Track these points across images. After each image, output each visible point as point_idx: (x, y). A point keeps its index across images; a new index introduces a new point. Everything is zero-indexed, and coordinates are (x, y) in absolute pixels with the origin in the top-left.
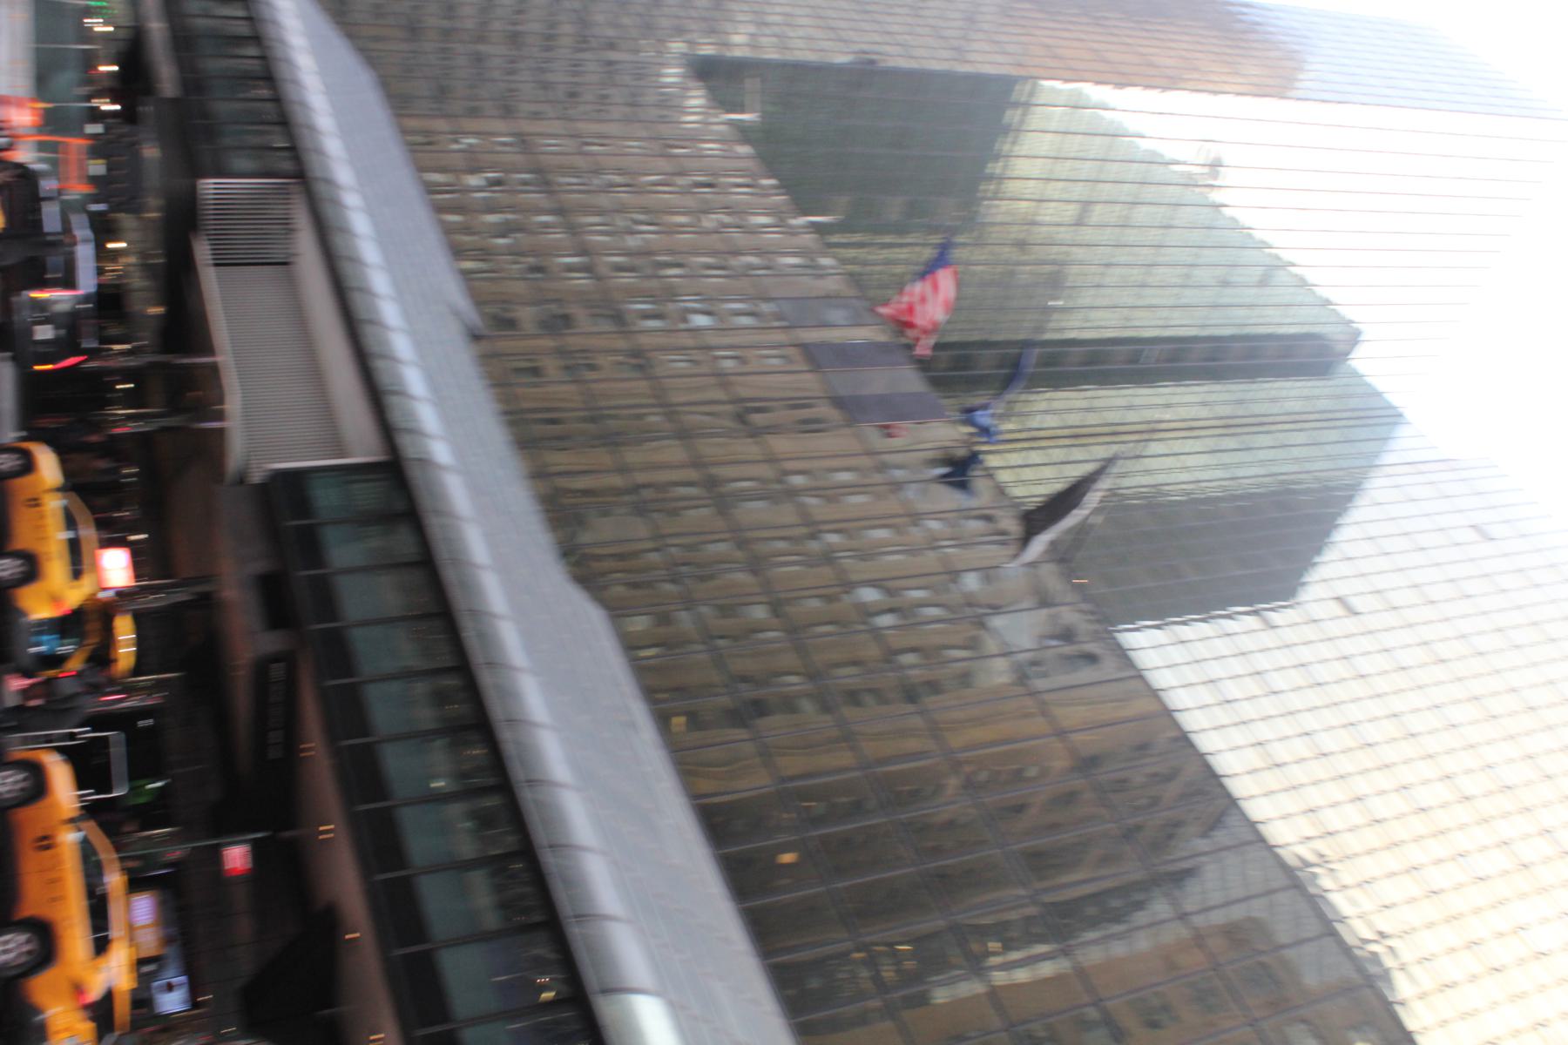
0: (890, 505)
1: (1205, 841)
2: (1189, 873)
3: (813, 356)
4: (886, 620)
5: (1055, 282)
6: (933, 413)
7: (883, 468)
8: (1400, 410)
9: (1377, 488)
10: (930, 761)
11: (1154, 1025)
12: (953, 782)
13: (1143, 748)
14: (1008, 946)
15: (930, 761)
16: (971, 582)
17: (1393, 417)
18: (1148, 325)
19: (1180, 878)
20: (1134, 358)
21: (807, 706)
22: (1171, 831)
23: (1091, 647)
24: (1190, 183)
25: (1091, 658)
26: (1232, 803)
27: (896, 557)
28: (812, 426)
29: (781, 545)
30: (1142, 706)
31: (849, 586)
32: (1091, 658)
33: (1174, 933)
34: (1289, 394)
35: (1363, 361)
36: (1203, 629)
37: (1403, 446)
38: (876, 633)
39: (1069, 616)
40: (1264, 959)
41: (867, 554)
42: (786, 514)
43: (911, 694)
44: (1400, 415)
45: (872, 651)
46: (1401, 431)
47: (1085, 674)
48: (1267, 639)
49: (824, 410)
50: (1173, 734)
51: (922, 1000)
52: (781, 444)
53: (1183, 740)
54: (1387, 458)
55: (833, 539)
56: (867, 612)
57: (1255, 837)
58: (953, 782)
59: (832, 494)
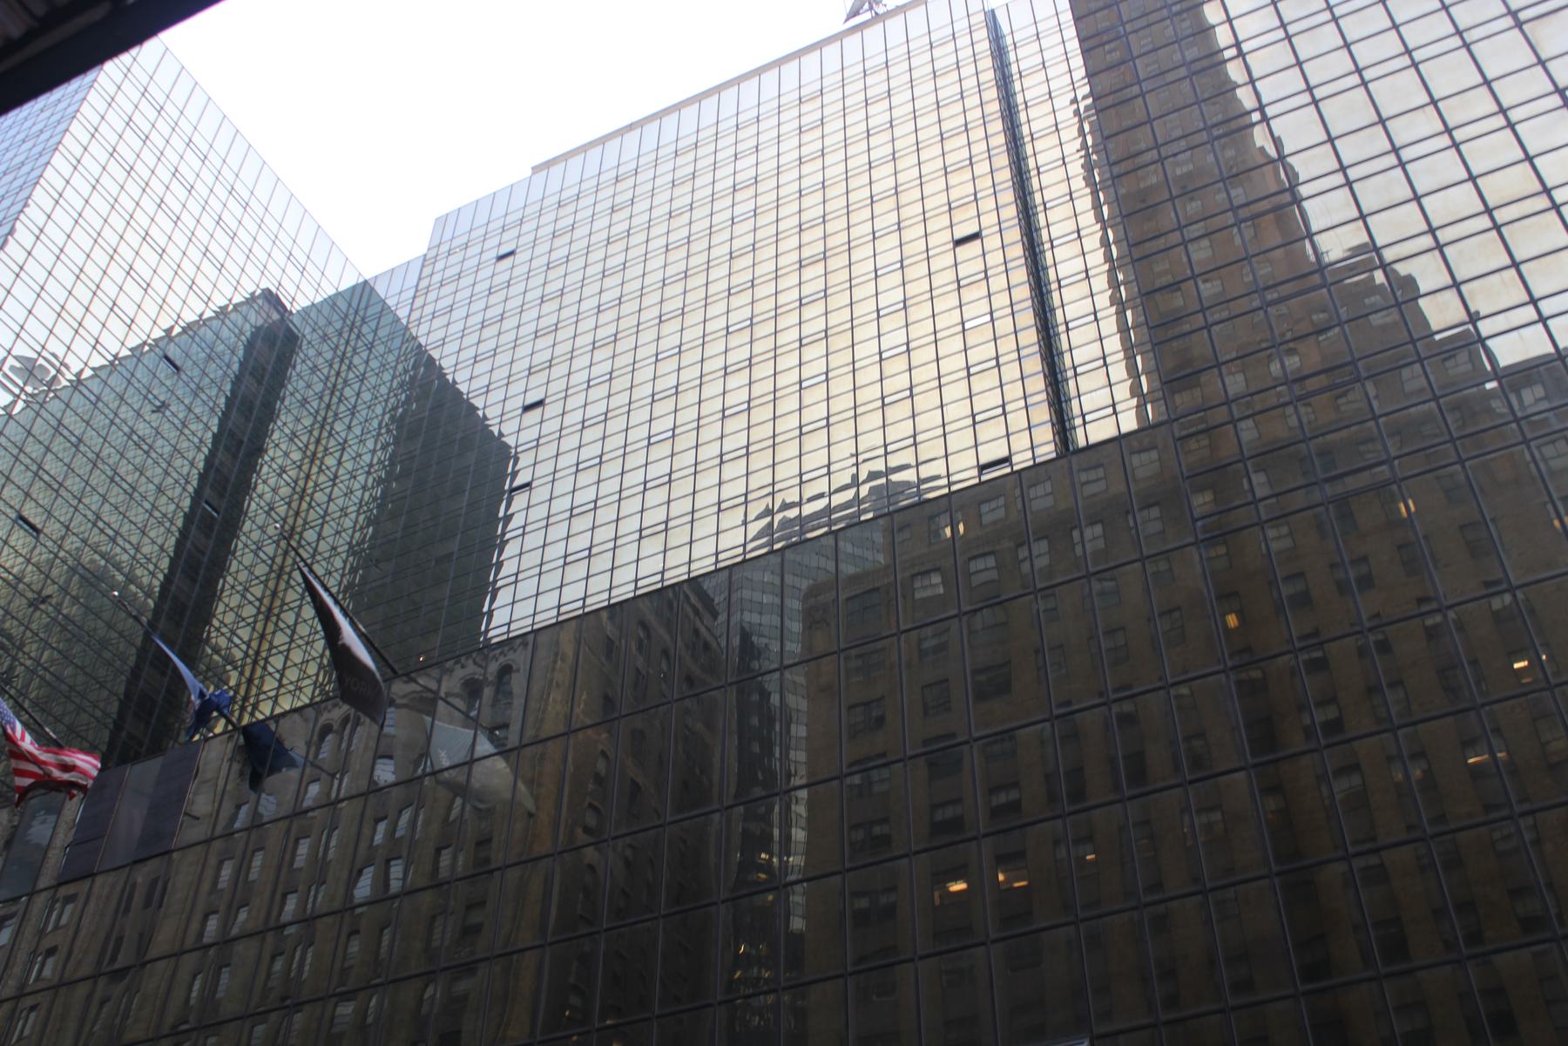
0: (275, 835)
1: (720, 617)
2: (745, 636)
3: (78, 872)
4: (396, 870)
5: (93, 579)
6: (191, 756)
7: (229, 835)
8: (361, 280)
9: (428, 335)
10: (557, 879)
11: (880, 721)
12: (590, 854)
13: (610, 646)
14: (765, 842)
15: (557, 879)
16: (385, 773)
17: (364, 290)
18: (192, 461)
19: (748, 648)
20: (207, 525)
21: (462, 986)
22: (700, 646)
23: (493, 667)
24: (36, 404)
25: (506, 670)
26: (694, 582)
27: (333, 843)
28: (156, 895)
29: (278, 965)
30: (567, 638)
31: (349, 907)
32: (506, 670)
33: (797, 677)
34: (303, 381)
35: (300, 296)
36: (511, 550)
37: (396, 297)
38: (407, 893)
39: (451, 684)
40: (842, 597)
41: (319, 869)
42: (245, 951)
43: (482, 869)
44: (366, 282)
45: (427, 899)
46: (381, 290)
47: (517, 683)
48: (540, 494)
49: (141, 876)
50: (604, 615)
51: (796, 939)
52: (163, 940)
53: (614, 609)
54: (402, 313)
55: (291, 904)
56: (383, 895)
57: (731, 574)
58: (590, 854)
59: (241, 896)
